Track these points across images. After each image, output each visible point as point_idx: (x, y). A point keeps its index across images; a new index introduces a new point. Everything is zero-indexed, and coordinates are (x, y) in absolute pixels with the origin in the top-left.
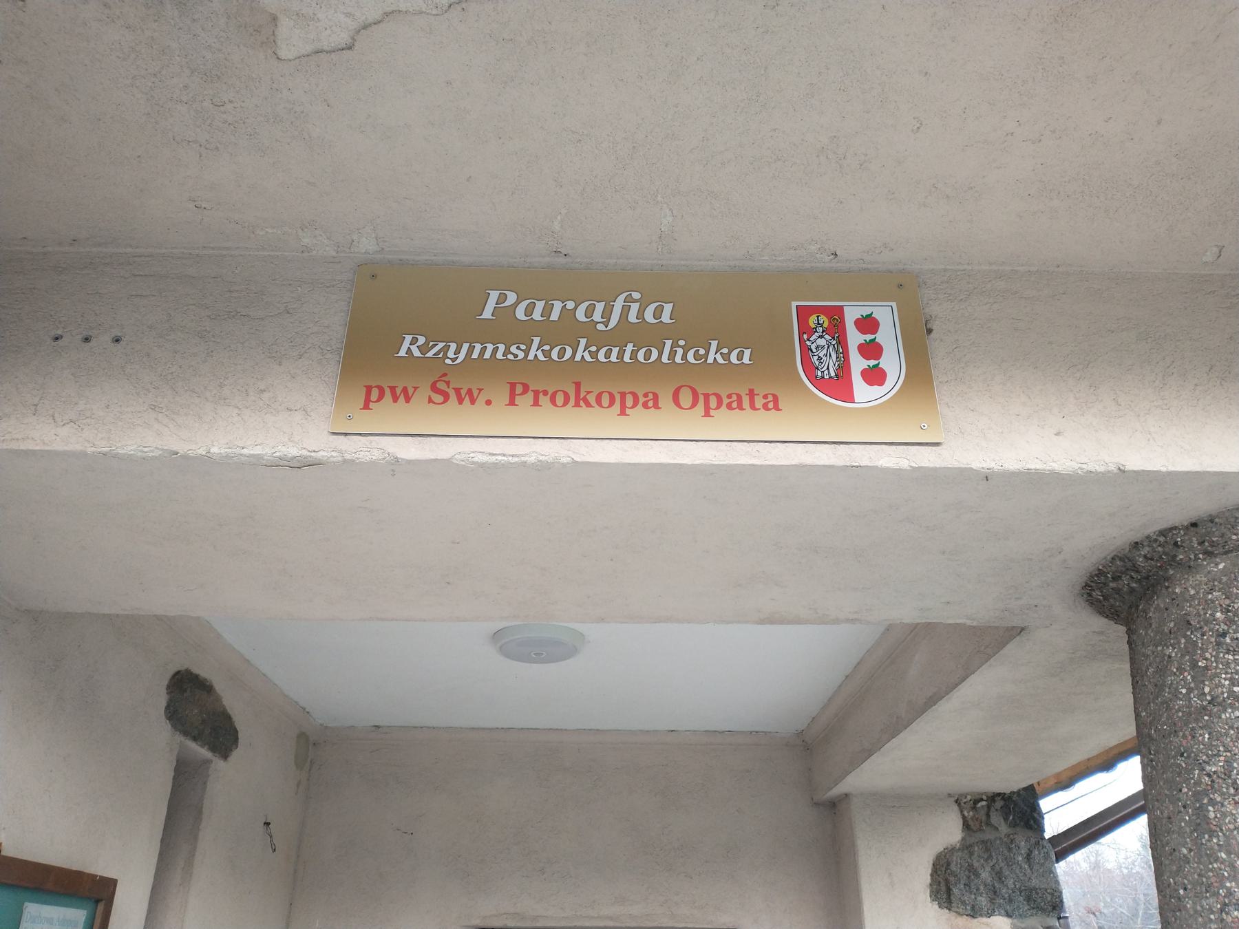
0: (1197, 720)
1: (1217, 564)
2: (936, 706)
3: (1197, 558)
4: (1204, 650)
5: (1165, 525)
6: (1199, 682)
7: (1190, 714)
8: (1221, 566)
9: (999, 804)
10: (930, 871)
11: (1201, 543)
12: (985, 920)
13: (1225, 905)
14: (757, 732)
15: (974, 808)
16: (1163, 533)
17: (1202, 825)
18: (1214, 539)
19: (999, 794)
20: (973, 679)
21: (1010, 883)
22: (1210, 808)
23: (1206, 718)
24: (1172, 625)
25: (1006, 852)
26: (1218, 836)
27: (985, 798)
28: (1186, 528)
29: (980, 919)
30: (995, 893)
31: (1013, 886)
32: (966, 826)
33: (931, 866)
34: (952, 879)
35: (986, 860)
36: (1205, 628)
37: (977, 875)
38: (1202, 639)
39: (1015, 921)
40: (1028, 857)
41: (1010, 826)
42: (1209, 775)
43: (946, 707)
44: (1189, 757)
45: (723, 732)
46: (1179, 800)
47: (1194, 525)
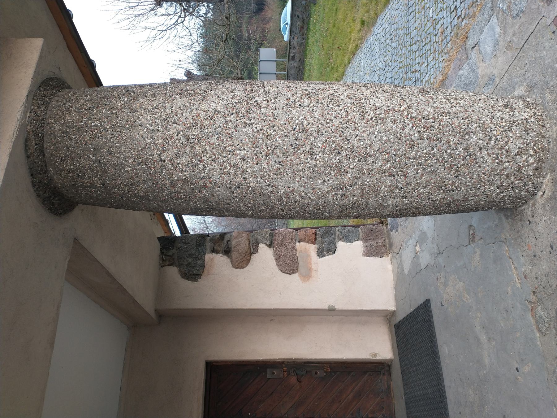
0: (110, 191)
1: (51, 171)
2: (112, 273)
3: (47, 176)
4: (84, 183)
5: (30, 184)
6: (95, 187)
7: (107, 192)
8: (52, 170)
9: (165, 251)
10: (187, 281)
11: (40, 174)
12: (206, 262)
13: (171, 197)
14: (126, 348)
15: (165, 261)
16: (34, 186)
17: (146, 197)
18: (39, 169)
19: (161, 250)
20: (99, 258)
21: (194, 252)
22: (140, 194)
23: (109, 188)
24: (73, 190)
25: (183, 251)
26: (149, 194)
27: (162, 256)
28: (33, 178)
29: (205, 265)
30: (197, 258)
31: (195, 251)
32: (172, 265)
33: (185, 280)
34: (190, 273)
35: (185, 259)
36: (75, 180)
37: (190, 263)
38: (79, 182)
39: (207, 252)
40: (185, 244)
41: (173, 248)
42: (129, 192)
43: (112, 269)
44: (123, 196)
45: (124, 363)
46: (138, 202)
47: (32, 175)
